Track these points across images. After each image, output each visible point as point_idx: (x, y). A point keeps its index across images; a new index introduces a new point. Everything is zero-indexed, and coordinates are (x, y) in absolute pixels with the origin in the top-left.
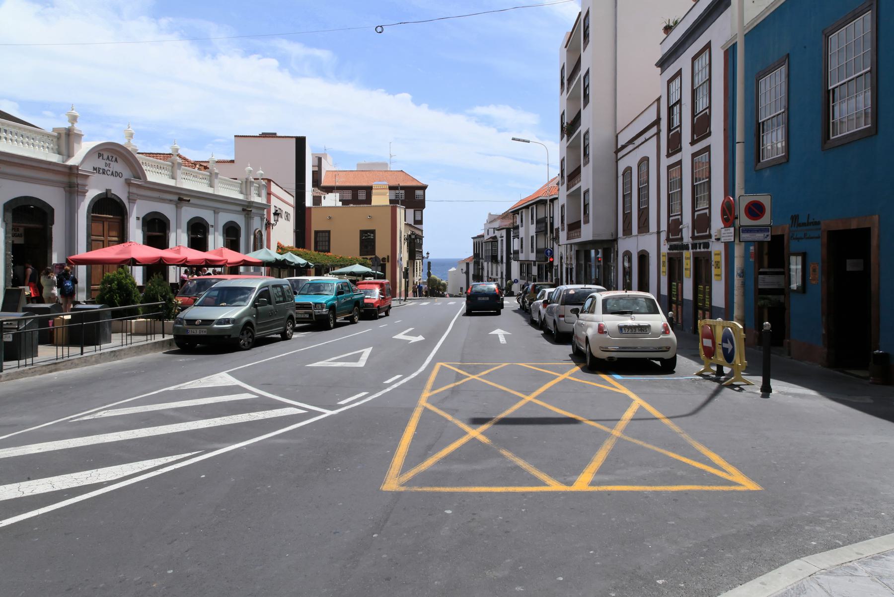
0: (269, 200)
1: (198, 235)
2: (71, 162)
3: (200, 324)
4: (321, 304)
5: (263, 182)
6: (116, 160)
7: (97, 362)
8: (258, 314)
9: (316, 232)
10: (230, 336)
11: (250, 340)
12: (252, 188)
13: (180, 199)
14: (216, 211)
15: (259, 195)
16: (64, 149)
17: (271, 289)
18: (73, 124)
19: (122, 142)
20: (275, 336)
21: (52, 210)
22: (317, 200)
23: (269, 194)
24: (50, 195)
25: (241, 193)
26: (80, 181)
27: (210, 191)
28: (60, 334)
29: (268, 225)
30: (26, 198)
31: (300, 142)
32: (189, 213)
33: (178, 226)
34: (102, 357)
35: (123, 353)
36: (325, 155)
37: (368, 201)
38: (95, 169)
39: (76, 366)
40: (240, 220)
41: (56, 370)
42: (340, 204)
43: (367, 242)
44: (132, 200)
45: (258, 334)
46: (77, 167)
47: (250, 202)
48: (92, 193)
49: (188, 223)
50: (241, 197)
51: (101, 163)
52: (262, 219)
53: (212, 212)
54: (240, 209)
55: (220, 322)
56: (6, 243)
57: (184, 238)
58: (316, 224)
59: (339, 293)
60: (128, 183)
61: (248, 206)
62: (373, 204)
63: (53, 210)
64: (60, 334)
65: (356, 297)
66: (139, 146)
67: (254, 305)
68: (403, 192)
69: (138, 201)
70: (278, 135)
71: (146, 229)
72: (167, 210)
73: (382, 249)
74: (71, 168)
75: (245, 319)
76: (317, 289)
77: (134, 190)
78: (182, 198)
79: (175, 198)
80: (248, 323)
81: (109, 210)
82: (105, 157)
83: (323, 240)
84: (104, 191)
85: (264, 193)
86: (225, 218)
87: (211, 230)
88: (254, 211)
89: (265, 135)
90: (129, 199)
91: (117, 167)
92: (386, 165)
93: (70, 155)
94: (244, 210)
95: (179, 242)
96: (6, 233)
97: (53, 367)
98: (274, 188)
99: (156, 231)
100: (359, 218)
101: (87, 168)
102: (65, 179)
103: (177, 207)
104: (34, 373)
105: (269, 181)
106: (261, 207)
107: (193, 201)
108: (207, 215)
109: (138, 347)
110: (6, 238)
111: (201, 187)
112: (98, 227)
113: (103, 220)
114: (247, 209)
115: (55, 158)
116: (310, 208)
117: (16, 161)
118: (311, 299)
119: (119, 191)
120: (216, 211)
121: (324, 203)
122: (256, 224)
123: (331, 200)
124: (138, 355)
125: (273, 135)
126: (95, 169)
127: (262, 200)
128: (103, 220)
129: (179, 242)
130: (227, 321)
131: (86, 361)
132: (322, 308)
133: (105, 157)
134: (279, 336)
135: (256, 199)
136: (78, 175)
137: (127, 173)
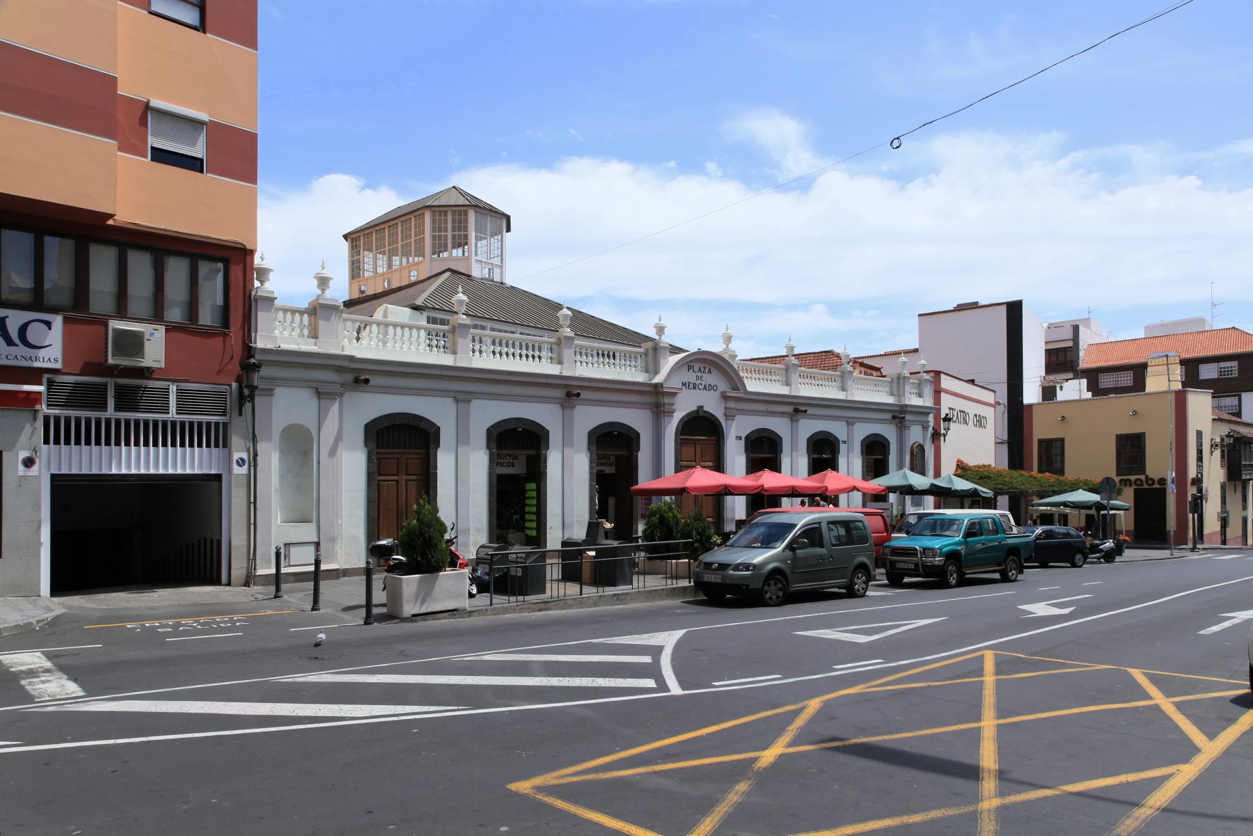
0: (937, 401)
1: (764, 451)
2: (658, 379)
3: (717, 569)
4: (932, 549)
5: (927, 377)
6: (710, 371)
7: (595, 604)
8: (795, 559)
9: (1041, 442)
10: (747, 586)
11: (780, 594)
12: (907, 388)
13: (796, 411)
14: (850, 423)
15: (920, 395)
16: (895, 391)
17: (824, 527)
18: (323, 290)
19: (717, 347)
20: (836, 590)
21: (546, 433)
22: (1049, 393)
23: (938, 392)
24: (635, 418)
25: (892, 394)
26: (666, 400)
27: (841, 396)
28: (586, 571)
29: (936, 436)
30: (610, 424)
31: (1014, 310)
32: (809, 427)
33: (567, 442)
34: (617, 598)
35: (628, 597)
36: (1087, 321)
37: (1139, 384)
38: (684, 384)
39: (570, 607)
40: (888, 432)
41: (546, 609)
42: (1089, 395)
43: (1131, 449)
44: (730, 417)
45: (797, 587)
46: (661, 385)
47: (902, 406)
48: (678, 415)
49: (809, 440)
50: (890, 400)
51: (691, 377)
52: (925, 428)
53: (844, 423)
54: (888, 416)
55: (737, 567)
56: (591, 473)
57: (803, 462)
58: (1041, 429)
59: (970, 533)
60: (725, 397)
61: (901, 412)
62: (1149, 389)
63: (488, 430)
64: (586, 571)
65: (1010, 541)
66: (743, 350)
67: (790, 547)
68: (1235, 364)
69: (738, 418)
70: (982, 303)
71: (594, 448)
72: (779, 425)
73: (1159, 464)
74: (656, 386)
75: (771, 566)
76: (939, 527)
77: (732, 404)
78: (798, 408)
79: (790, 409)
80: (776, 571)
81: (702, 434)
82: (696, 369)
83: (1053, 453)
84: (695, 408)
85: (928, 390)
86: (863, 430)
87: (843, 448)
88: (908, 417)
89: (961, 308)
90: (726, 415)
91: (710, 379)
92: (1202, 321)
93: (656, 372)
94: (894, 417)
95: (794, 468)
96: (591, 462)
97: (543, 606)
98: (946, 383)
99: (764, 451)
100: (1119, 415)
101: (675, 383)
102: (651, 399)
103: (563, 407)
104: (521, 610)
105: (938, 374)
106: (922, 412)
107: (584, 395)
108: (837, 429)
109: (650, 592)
110: (591, 467)
111: (830, 392)
112: (688, 451)
113: (695, 442)
114: (899, 415)
115: (640, 377)
116: (1030, 406)
117: (438, 372)
118: (918, 543)
119: (713, 406)
120: (850, 423)
121: (1061, 396)
122: (915, 435)
123: (1073, 390)
124: (649, 601)
125: (974, 306)
126: (684, 384)
127: (927, 401)
128: (695, 442)
129: (794, 468)
130: (747, 567)
131: (600, 600)
132: (934, 556)
133: (696, 369)
134: (997, 576)
135: (915, 401)
136: (664, 394)
137: (723, 386)
